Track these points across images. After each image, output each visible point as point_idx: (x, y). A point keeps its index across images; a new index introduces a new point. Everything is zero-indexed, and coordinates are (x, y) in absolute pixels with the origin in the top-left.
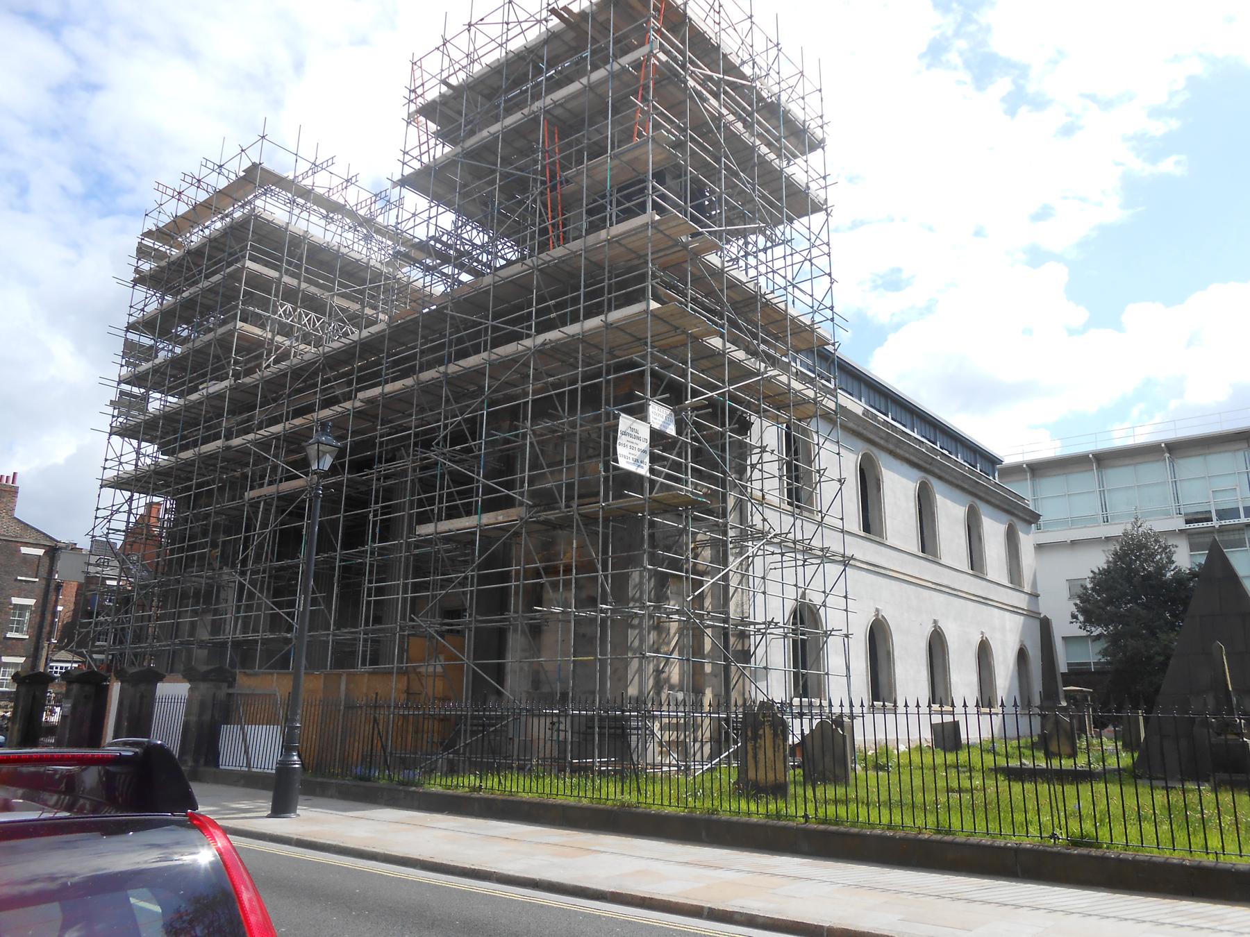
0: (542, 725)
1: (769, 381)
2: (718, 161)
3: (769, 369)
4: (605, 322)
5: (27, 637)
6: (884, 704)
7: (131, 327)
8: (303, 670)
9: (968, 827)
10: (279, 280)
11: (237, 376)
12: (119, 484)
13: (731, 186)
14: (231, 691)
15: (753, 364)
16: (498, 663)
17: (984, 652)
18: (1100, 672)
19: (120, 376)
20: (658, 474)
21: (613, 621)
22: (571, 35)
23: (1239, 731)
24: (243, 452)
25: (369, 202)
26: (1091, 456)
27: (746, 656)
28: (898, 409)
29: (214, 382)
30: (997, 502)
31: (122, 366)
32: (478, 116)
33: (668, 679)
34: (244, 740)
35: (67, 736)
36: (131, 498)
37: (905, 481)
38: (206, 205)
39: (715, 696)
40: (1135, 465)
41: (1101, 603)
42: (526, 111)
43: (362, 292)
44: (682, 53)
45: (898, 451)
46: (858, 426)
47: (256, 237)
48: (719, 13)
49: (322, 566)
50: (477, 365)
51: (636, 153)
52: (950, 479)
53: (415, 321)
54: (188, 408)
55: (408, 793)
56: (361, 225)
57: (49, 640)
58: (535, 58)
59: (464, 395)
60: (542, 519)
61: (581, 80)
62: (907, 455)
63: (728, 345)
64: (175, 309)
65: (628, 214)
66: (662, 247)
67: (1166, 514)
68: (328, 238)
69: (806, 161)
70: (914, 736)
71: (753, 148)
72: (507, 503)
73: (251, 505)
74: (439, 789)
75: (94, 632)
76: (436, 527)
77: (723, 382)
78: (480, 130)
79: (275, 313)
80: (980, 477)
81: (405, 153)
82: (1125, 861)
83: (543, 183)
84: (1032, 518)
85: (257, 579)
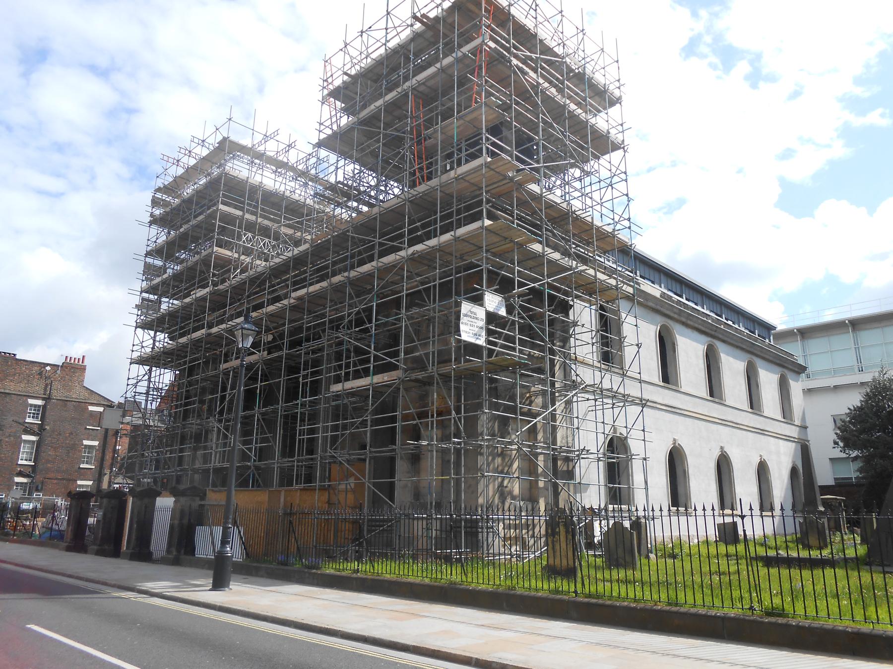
0: (420, 527)
1: (580, 274)
3: (579, 265)
4: (454, 236)
5: (94, 467)
6: (678, 509)
7: (148, 254)
10: (243, 216)
12: (141, 361)
14: (203, 503)
15: (566, 262)
17: (762, 471)
18: (858, 485)
19: (141, 288)
20: (495, 344)
21: (466, 451)
22: (429, 34)
24: (219, 336)
26: (847, 322)
28: (691, 292)
29: (200, 289)
30: (771, 358)
31: (143, 281)
35: (100, 535)
37: (695, 344)
40: (882, 327)
41: (855, 433)
42: (399, 90)
43: (301, 223)
44: (508, 42)
45: (689, 322)
48: (536, 10)
50: (370, 271)
52: (732, 342)
54: (185, 307)
55: (310, 574)
56: (299, 176)
58: (406, 51)
59: (364, 292)
60: (413, 378)
62: (696, 325)
63: (546, 249)
64: (176, 240)
65: (473, 156)
68: (277, 186)
69: (607, 114)
70: (702, 533)
71: (564, 106)
72: (395, 367)
73: (224, 374)
74: (332, 571)
76: (343, 386)
77: (543, 276)
80: (756, 340)
81: (321, 124)
82: (803, 628)
83: (412, 139)
84: (799, 370)
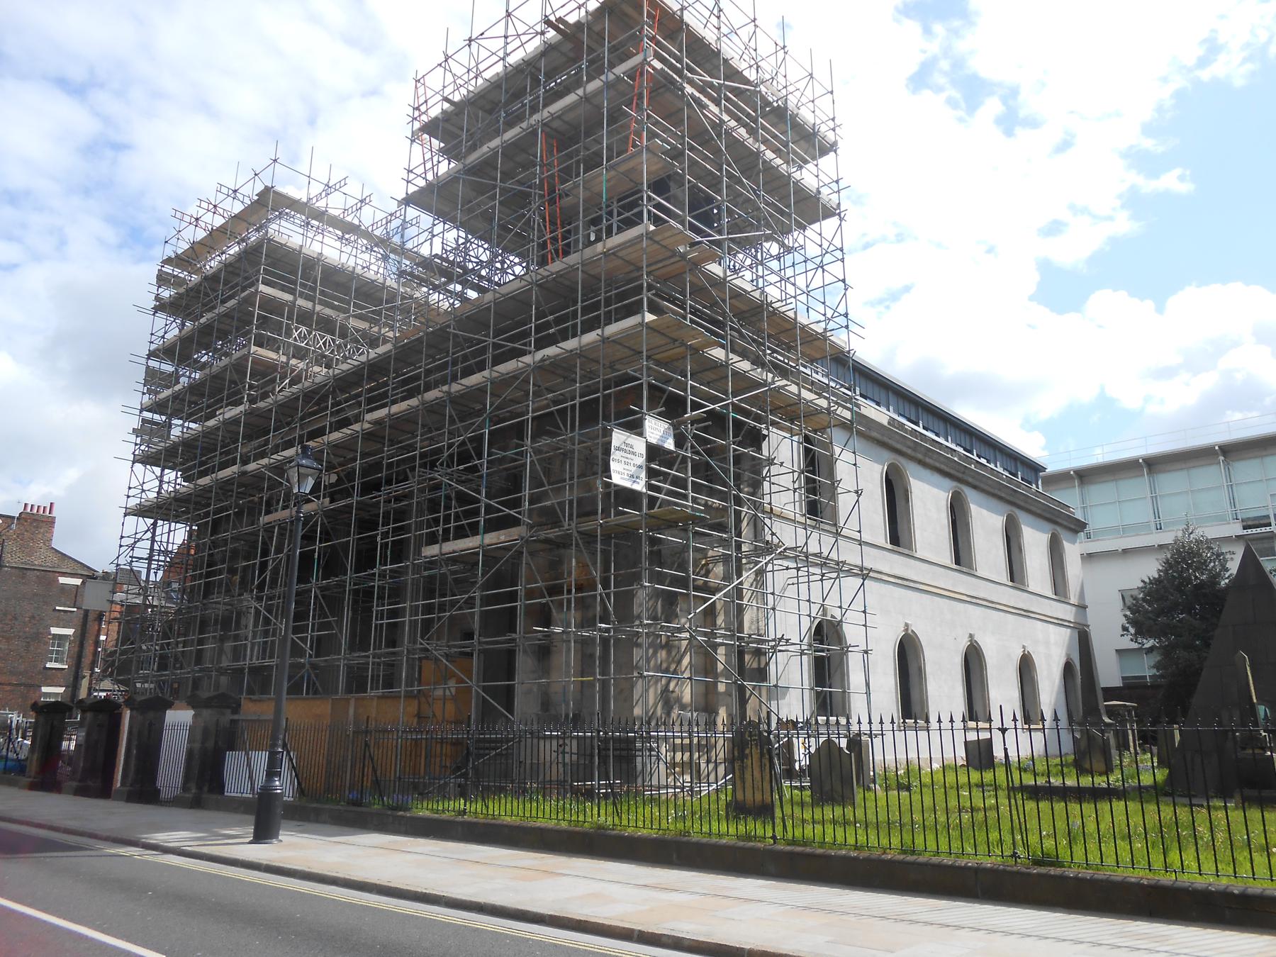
1: (778, 391)
2: (720, 170)
3: (776, 379)
5: (67, 667)
7: (151, 355)
8: (284, 695)
9: (932, 845)
10: (294, 303)
11: (252, 400)
13: (735, 197)
14: (236, 717)
15: (758, 374)
16: (508, 685)
17: (1026, 667)
20: (658, 490)
21: (617, 641)
23: (1264, 745)
24: (258, 476)
25: (384, 222)
26: (1141, 461)
27: (762, 674)
28: (930, 417)
29: (230, 407)
30: (1039, 511)
31: (144, 394)
32: (479, 131)
33: (679, 700)
34: (249, 765)
35: (82, 765)
36: (155, 525)
37: (935, 490)
38: (222, 230)
39: (730, 715)
40: (1188, 468)
41: (1151, 615)
42: (524, 125)
43: (379, 313)
44: (679, 60)
46: (883, 435)
47: (270, 260)
49: (335, 590)
50: (480, 383)
51: (631, 164)
52: (986, 488)
53: (419, 340)
54: (206, 434)
56: (376, 245)
57: (92, 669)
59: (470, 414)
61: (577, 92)
62: (938, 465)
63: (731, 356)
64: (193, 334)
66: (660, 257)
67: (1220, 519)
68: (344, 260)
69: (817, 165)
70: (949, 755)
71: (758, 154)
72: (510, 522)
73: (265, 530)
74: (427, 814)
75: (119, 661)
77: (726, 393)
78: (482, 145)
79: (289, 335)
81: (410, 171)
83: (542, 196)
84: (1077, 527)
85: (273, 605)
